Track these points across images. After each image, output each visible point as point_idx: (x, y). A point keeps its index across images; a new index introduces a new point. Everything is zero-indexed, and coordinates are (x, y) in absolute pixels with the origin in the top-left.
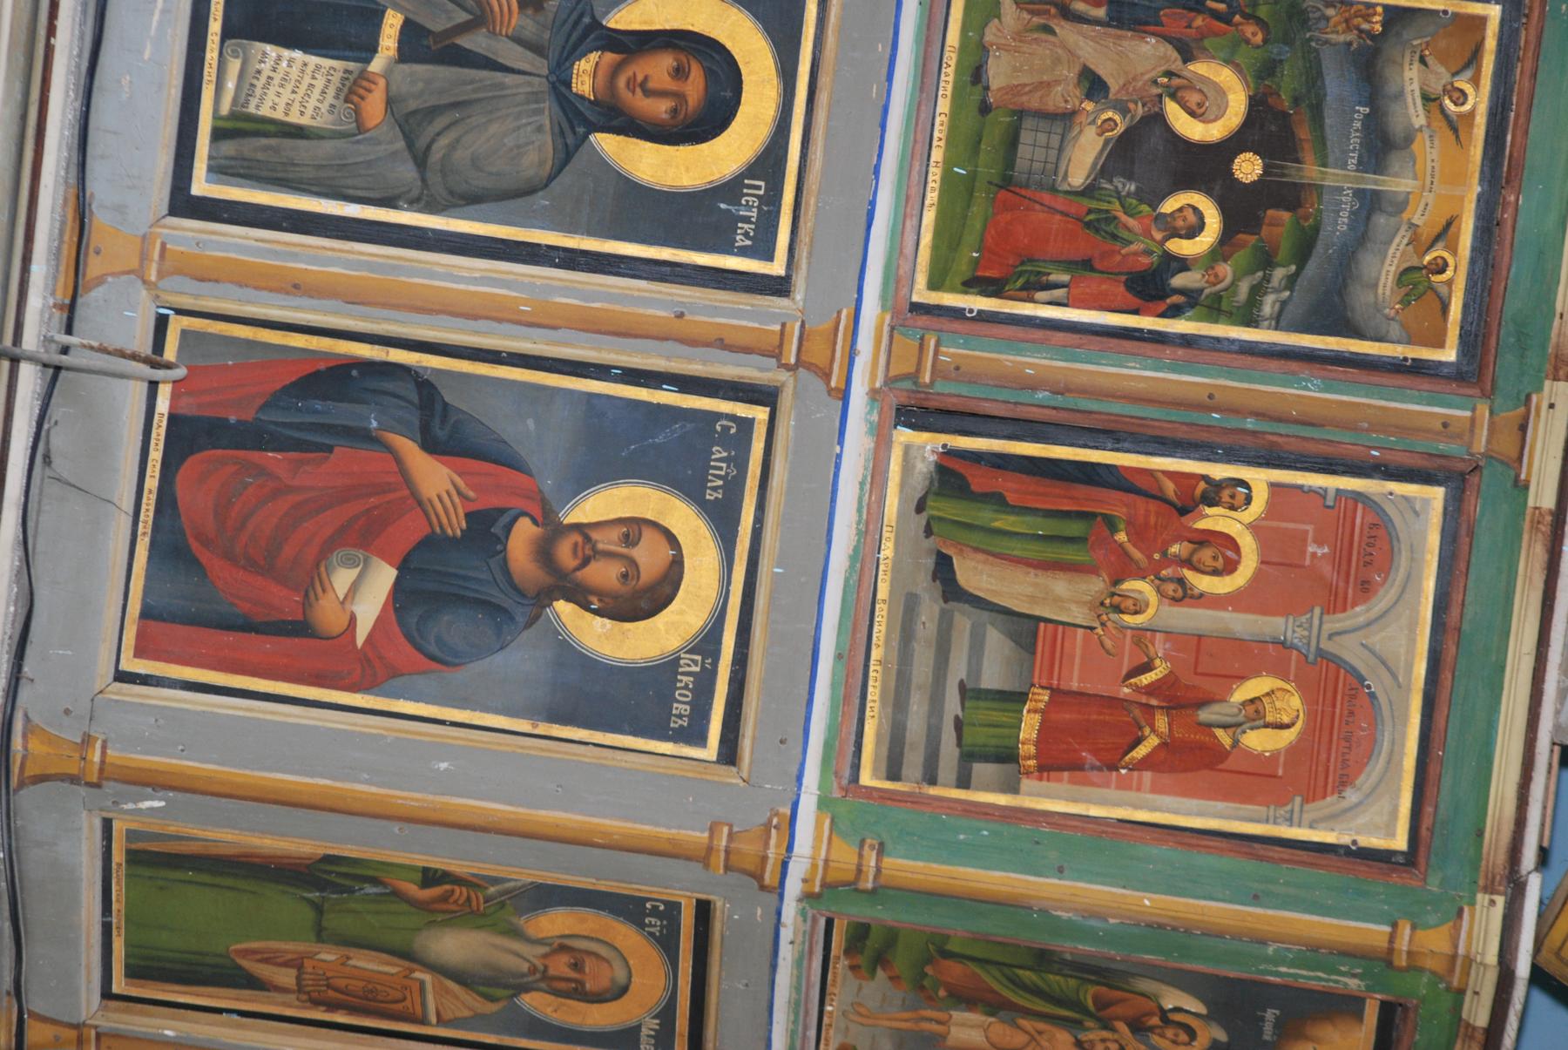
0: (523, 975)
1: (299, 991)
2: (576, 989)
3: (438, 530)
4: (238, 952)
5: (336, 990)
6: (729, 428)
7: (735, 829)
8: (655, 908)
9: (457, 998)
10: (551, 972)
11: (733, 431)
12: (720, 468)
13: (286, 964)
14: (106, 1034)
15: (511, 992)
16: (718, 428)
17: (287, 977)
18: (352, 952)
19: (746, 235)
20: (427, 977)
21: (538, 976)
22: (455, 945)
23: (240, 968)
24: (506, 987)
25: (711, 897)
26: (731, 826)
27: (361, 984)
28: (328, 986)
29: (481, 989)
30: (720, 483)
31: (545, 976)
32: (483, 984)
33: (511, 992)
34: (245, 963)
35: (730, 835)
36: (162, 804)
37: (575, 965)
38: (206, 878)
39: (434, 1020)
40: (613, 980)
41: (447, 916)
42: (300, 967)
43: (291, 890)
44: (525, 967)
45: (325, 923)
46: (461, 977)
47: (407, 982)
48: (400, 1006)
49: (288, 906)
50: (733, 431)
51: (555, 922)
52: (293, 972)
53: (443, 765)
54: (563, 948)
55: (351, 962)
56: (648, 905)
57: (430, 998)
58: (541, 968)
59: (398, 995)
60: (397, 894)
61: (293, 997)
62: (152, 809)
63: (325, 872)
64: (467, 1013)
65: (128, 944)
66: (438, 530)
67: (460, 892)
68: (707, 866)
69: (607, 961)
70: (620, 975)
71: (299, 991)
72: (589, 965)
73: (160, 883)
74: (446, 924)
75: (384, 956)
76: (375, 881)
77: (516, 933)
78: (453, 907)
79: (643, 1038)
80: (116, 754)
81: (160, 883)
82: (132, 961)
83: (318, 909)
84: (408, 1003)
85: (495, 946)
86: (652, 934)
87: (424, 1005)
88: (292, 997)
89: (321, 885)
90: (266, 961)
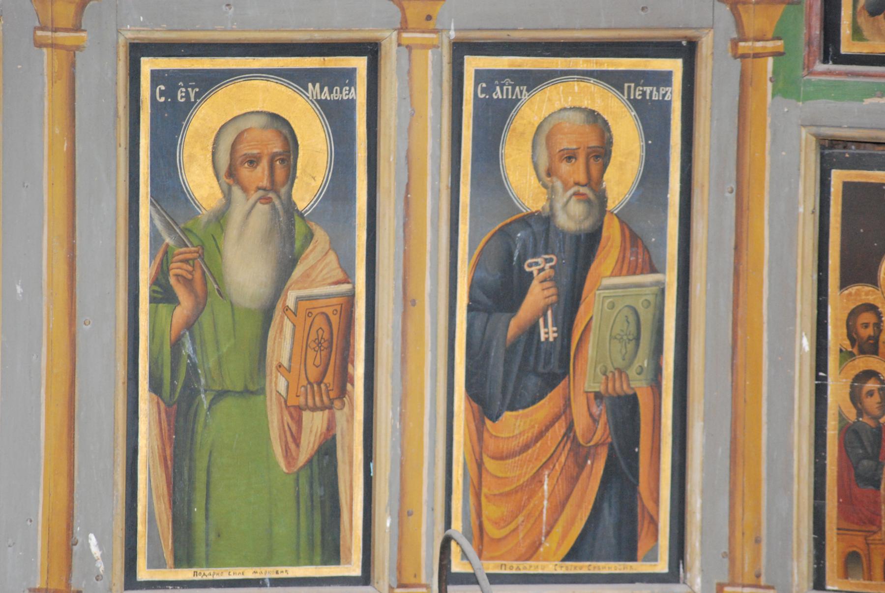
0: (274, 208)
1: (330, 408)
2: (282, 161)
3: (334, 301)
4: (289, 464)
5: (324, 374)
6: (482, 88)
7: (37, 24)
8: (483, 91)
9: (313, 267)
10: (265, 183)
11: (163, 88)
12: (507, 89)
13: (299, 422)
14: (399, 580)
15: (297, 219)
16: (163, 99)
17: (314, 424)
18: (271, 361)
19: (322, 90)
20: (291, 298)
21: (271, 195)
22: (246, 269)
23: (310, 462)
24: (291, 224)
25: (121, 41)
26: (36, 29)
27: (311, 354)
28: (319, 384)
29: (298, 244)
30: (517, 88)
31: (273, 187)
32: (292, 244)
33: (297, 219)
34: (303, 458)
35: (42, 28)
36: (92, 537)
37: (251, 162)
38: (199, 497)
39: (345, 287)
40: (264, 128)
41: (210, 279)
42: (300, 409)
43: (201, 419)
44: (262, 209)
45: (239, 387)
46: (286, 265)
47: (302, 313)
48: (335, 319)
49: (218, 424)
50: (163, 88)
51: (201, 182)
52: (306, 415)
53: (19, 289)
54: (232, 172)
55: (285, 363)
56: (482, 96)
57: (316, 291)
58: (261, 193)
59: (319, 322)
60: (190, 325)
61: (338, 414)
62: (100, 545)
63: (173, 387)
64: (332, 257)
65: (297, 563)
66: (334, 301)
67: (176, 269)
68: (78, 48)
69: (240, 136)
70: (255, 122)
71: (330, 408)
72: (245, 149)
73: (212, 536)
74: (219, 279)
75: (271, 333)
76: (177, 345)
77: (220, 217)
78: (198, 275)
79: (335, 96)
80: (39, 578)
81: (212, 536)
82: (318, 559)
83: (222, 394)
84: (329, 311)
85: (241, 234)
86: (198, 95)
87: (328, 296)
88: (340, 416)
89: (190, 393)
90: (297, 441)
